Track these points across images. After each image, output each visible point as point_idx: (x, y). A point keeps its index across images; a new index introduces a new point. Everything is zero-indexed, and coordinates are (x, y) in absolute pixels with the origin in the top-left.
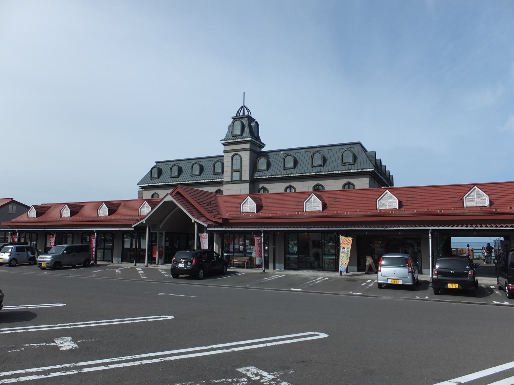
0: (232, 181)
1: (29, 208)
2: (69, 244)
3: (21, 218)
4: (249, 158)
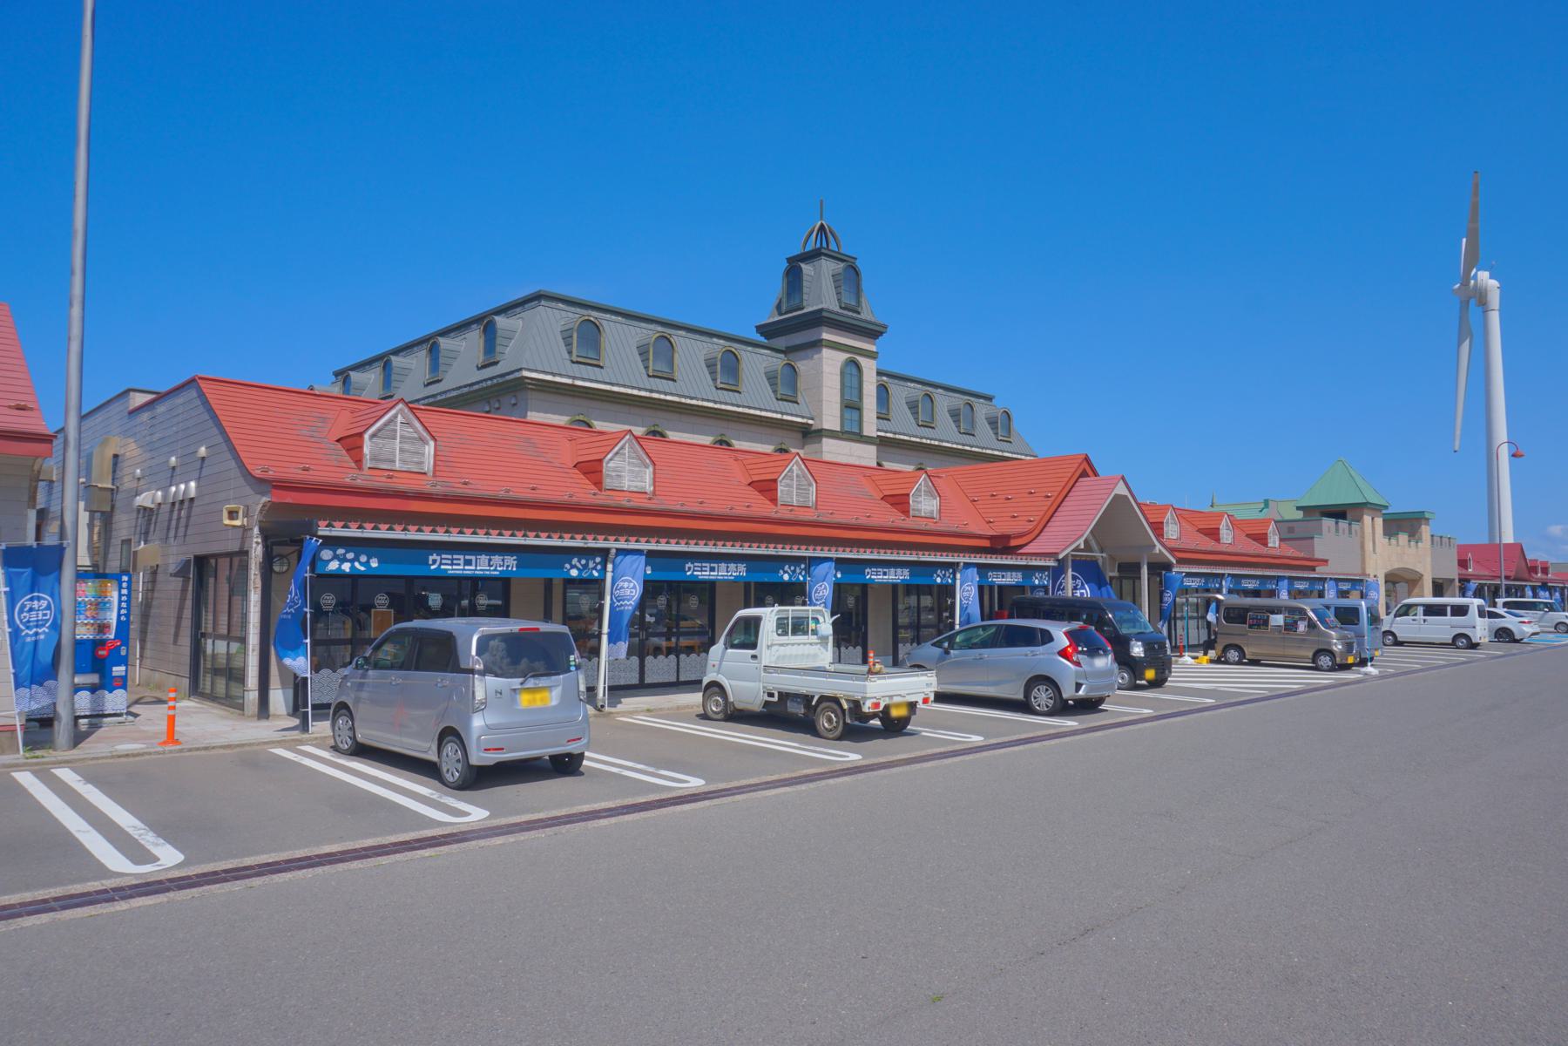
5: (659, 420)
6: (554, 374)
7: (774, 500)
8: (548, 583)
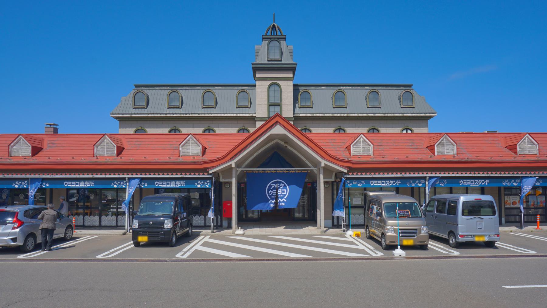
5: (408, 124)
6: (412, 113)
7: (516, 153)
8: (500, 188)
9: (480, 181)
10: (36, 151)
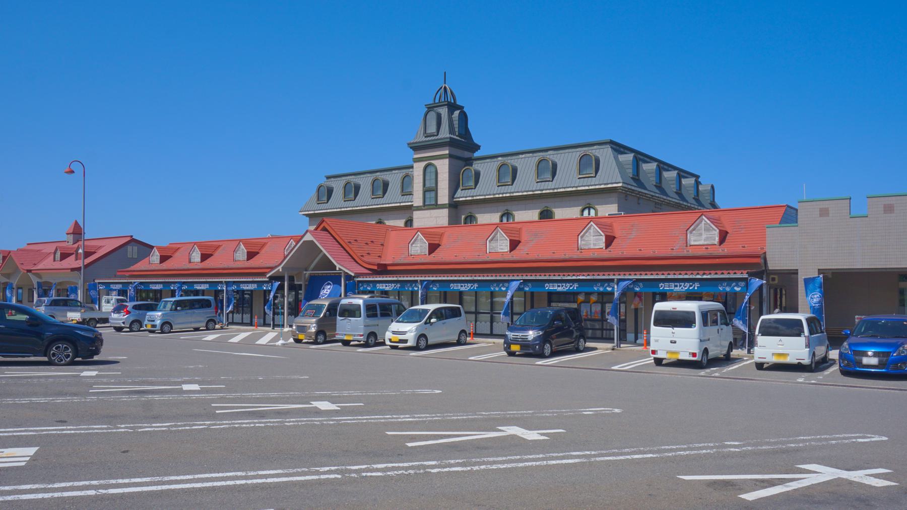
0: (424, 205)
1: (152, 247)
2: (177, 298)
3: (141, 266)
4: (447, 170)
9: (687, 284)
10: (433, 248)
